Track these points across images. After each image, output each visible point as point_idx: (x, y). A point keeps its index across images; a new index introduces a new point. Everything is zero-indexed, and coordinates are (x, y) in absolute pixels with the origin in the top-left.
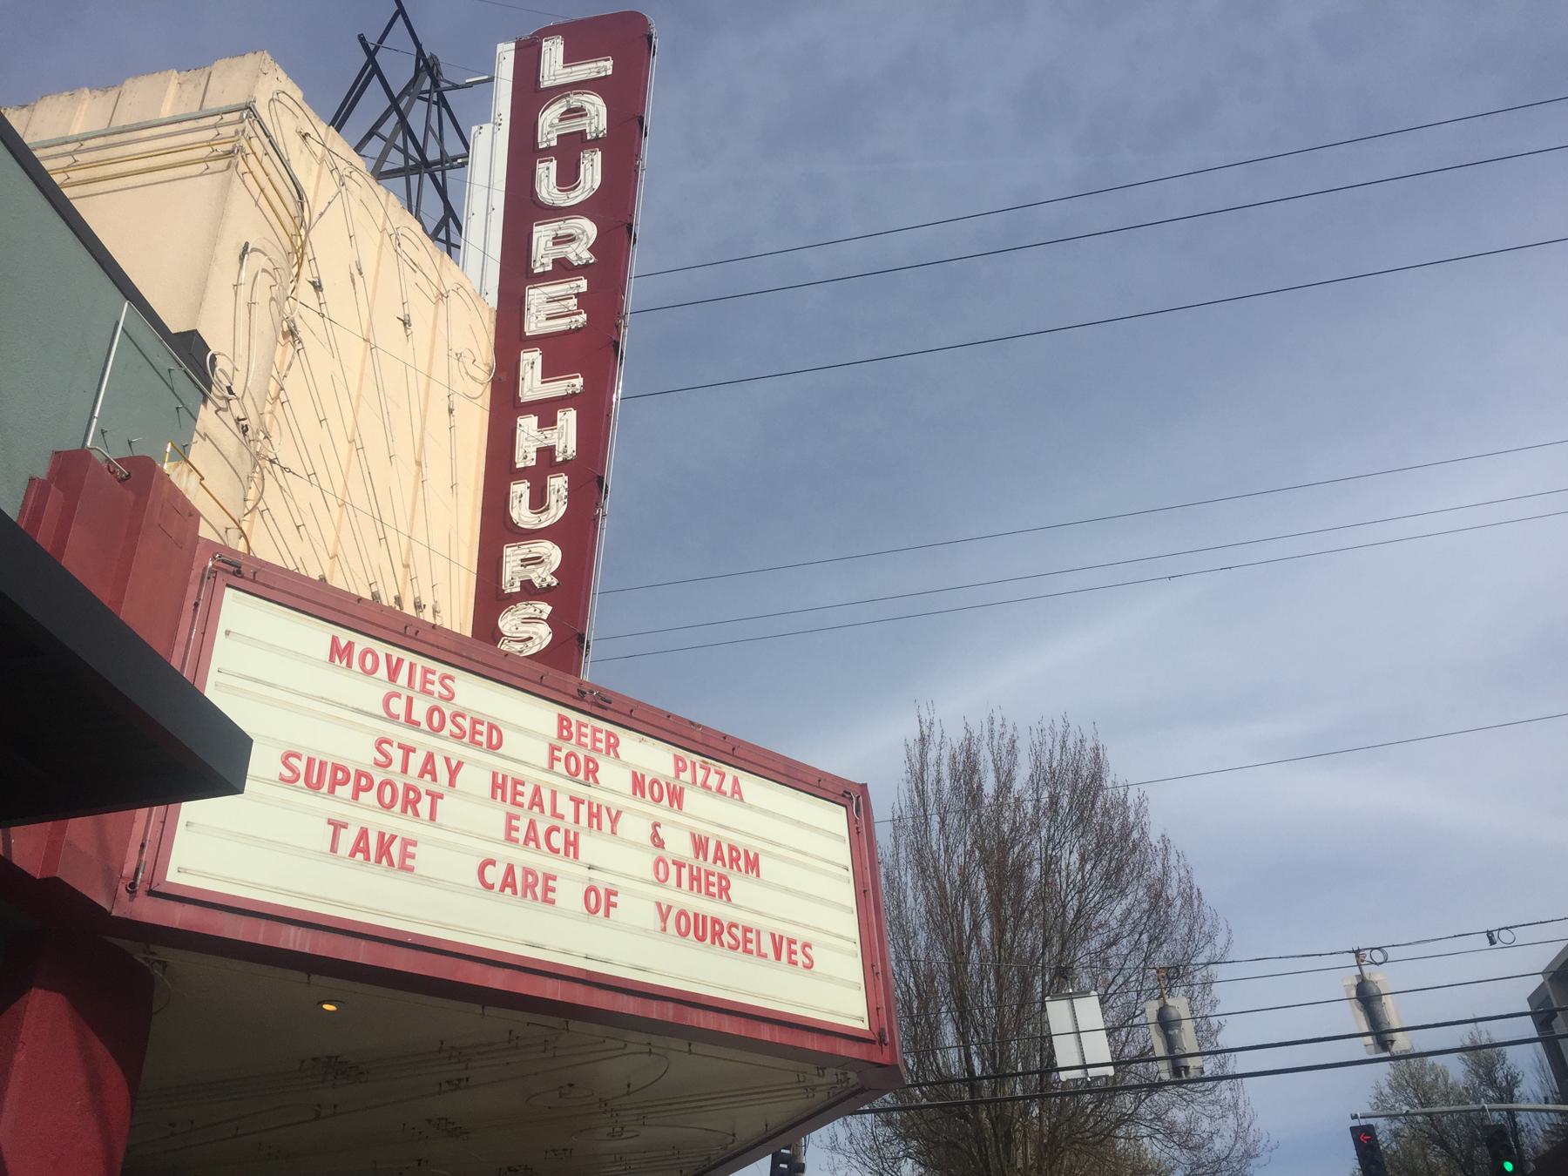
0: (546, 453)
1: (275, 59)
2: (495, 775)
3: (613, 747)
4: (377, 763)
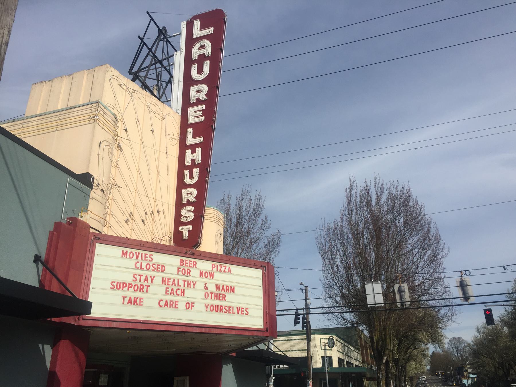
0: (193, 161)
1: (111, 66)
2: (163, 278)
3: (195, 265)
4: (133, 281)
